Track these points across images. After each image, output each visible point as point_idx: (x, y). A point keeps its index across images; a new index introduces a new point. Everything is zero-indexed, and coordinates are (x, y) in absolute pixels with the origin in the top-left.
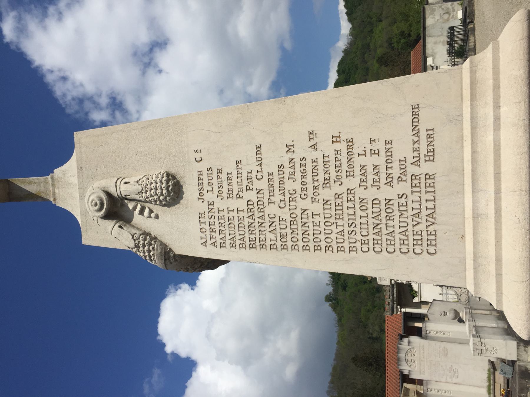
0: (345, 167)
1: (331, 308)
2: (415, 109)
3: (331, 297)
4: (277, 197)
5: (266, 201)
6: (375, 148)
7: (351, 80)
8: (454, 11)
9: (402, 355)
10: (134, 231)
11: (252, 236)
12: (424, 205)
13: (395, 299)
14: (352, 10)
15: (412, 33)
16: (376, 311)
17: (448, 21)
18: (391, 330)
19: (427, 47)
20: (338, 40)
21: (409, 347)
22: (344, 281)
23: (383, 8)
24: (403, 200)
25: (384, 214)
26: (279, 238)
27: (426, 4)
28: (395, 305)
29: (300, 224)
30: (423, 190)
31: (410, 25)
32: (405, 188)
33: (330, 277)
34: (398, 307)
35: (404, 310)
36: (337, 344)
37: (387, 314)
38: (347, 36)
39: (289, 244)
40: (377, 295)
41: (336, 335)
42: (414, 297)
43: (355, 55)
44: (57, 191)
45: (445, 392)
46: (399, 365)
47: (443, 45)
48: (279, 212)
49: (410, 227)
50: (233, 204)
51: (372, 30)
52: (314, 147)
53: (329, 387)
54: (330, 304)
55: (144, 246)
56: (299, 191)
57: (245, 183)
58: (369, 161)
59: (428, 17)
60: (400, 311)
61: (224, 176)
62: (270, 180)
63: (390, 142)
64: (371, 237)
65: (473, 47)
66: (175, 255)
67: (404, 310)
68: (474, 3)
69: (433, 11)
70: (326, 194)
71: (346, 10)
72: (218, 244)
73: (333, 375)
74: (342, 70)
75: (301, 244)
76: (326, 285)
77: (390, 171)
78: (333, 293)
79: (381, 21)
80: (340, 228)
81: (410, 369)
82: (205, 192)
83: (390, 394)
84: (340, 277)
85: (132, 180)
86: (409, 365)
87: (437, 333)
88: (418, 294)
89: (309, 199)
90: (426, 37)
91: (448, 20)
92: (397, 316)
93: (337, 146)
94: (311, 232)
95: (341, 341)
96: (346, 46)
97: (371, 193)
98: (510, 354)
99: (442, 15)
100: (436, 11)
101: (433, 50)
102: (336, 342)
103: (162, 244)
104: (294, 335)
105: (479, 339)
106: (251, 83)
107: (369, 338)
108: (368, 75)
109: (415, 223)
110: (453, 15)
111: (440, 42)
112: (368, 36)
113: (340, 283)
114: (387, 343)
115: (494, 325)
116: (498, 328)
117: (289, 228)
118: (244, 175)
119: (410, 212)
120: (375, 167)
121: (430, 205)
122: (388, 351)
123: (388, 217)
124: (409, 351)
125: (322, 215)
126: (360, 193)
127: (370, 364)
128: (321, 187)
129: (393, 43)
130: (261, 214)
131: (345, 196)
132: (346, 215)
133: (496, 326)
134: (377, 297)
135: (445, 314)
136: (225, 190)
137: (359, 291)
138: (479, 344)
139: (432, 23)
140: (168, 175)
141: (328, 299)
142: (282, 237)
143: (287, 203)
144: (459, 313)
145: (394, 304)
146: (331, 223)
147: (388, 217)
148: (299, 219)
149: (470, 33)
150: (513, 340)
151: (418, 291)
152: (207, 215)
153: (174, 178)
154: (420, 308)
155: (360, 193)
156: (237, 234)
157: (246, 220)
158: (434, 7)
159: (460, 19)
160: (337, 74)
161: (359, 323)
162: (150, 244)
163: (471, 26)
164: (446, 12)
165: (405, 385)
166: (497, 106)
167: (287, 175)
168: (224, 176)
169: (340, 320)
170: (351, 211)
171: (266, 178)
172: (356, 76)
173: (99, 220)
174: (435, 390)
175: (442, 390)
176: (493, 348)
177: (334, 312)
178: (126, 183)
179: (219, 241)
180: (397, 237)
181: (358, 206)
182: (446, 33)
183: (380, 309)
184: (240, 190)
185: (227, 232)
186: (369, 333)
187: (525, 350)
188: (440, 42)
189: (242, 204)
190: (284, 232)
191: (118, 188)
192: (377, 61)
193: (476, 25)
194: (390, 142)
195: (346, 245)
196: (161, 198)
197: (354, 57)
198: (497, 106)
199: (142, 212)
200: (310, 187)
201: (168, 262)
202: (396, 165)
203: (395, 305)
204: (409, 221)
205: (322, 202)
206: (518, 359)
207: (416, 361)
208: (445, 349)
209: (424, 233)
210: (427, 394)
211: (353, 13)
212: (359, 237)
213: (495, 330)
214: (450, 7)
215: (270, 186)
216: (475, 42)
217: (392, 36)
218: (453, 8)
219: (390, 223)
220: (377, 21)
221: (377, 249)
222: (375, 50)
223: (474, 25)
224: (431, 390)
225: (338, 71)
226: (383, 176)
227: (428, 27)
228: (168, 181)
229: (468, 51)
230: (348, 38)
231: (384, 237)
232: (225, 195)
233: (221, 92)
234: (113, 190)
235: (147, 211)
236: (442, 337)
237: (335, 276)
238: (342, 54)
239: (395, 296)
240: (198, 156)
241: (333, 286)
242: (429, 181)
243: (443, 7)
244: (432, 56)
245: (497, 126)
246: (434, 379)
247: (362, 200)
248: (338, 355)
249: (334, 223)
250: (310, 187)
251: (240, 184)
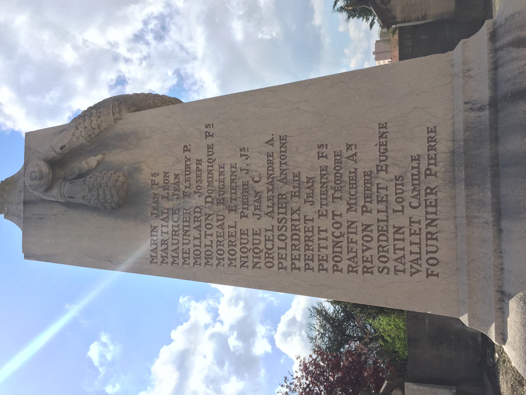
109: (414, 270)
146: (259, 249)
249: (250, 249)
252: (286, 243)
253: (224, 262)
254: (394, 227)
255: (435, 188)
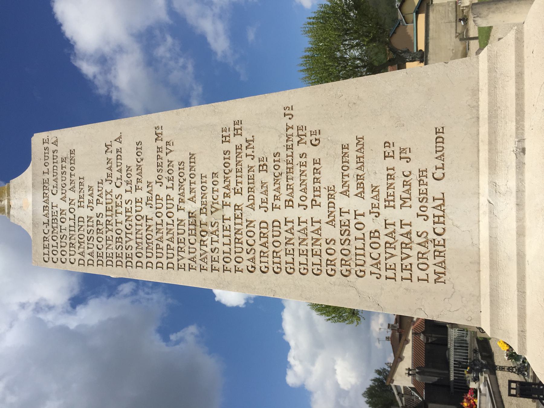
252: (75, 215)
253: (152, 246)
254: (247, 221)
255: (241, 205)
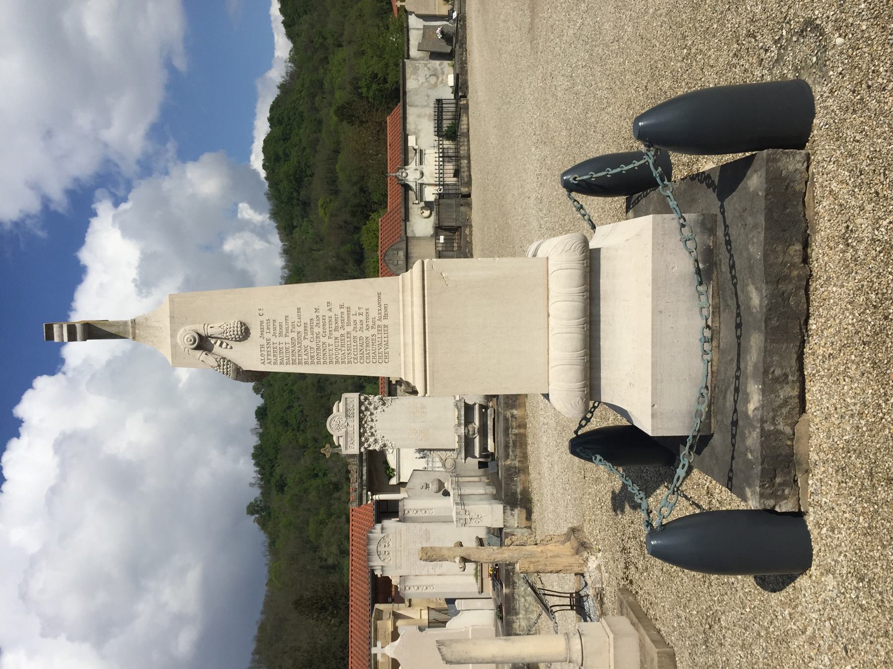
0: (346, 321)
1: (257, 525)
2: (379, 295)
3: (258, 506)
4: (309, 336)
5: (302, 338)
6: (361, 312)
7: (292, 137)
8: (443, 73)
9: (373, 547)
10: (216, 357)
11: (294, 358)
12: (383, 339)
13: (364, 482)
14: (294, 18)
15: (389, 80)
16: (333, 522)
17: (435, 86)
18: (357, 534)
19: (408, 121)
20: (269, 67)
21: (383, 535)
22: (281, 476)
23: (344, 25)
24: (374, 337)
25: (365, 344)
26: (310, 358)
27: (406, 58)
28: (364, 492)
29: (322, 350)
30: (383, 332)
31: (387, 66)
32: (375, 331)
33: (256, 472)
34: (369, 493)
35: (377, 497)
36: (267, 584)
37: (353, 506)
38: (286, 62)
39: (316, 361)
40: (336, 495)
41: (265, 570)
42: (391, 477)
43: (299, 95)
44: (137, 331)
45: (427, 588)
46: (369, 560)
47: (430, 121)
48: (310, 344)
49: (377, 350)
50: (283, 340)
51: (326, 58)
52: (330, 310)
53: (253, 661)
54: (256, 517)
55: (224, 365)
56: (322, 333)
57: (290, 328)
58: (358, 318)
59: (410, 78)
60: (372, 499)
61: (277, 324)
62: (305, 327)
63: (368, 309)
64: (358, 356)
65: (466, 131)
66: (243, 370)
67: (377, 497)
68: (467, 71)
69: (416, 69)
70: (336, 334)
71: (283, 18)
72: (272, 363)
73: (259, 640)
74: (278, 118)
75: (322, 361)
76: (248, 486)
77: (368, 323)
78: (261, 498)
79: (340, 46)
80: (343, 352)
81: (383, 564)
82: (265, 333)
83: (355, 631)
84: (274, 470)
85: (216, 325)
86: (382, 559)
87: (417, 512)
88: (395, 473)
89: (327, 337)
90: (407, 106)
91: (435, 85)
92: (367, 507)
93: (342, 310)
94: (328, 354)
95: (274, 579)
96: (283, 79)
97: (359, 334)
98: (496, 521)
99: (427, 76)
100: (420, 70)
101: (416, 125)
102: (266, 581)
103: (235, 364)
104: (193, 577)
105: (463, 506)
106: (108, 125)
107: (321, 567)
108: (320, 131)
110: (442, 80)
111: (425, 115)
112: (321, 67)
113: (273, 480)
114: (352, 555)
115: (482, 491)
116: (486, 494)
117: (315, 352)
118: (290, 324)
119: (377, 343)
120: (361, 321)
121: (386, 339)
122: (353, 568)
123: (367, 346)
124: (382, 540)
125: (334, 345)
126: (353, 334)
127: (323, 608)
128: (333, 331)
129: (360, 88)
130: (299, 345)
131: (346, 335)
132: (346, 345)
133: (484, 493)
134: (335, 499)
135: (427, 486)
136: (278, 331)
137: (306, 491)
138: (463, 512)
139: (414, 87)
140: (241, 323)
141: (252, 509)
142: (312, 357)
143: (315, 339)
144: (444, 483)
145: (362, 489)
147: (367, 346)
148: (321, 347)
149: (462, 110)
150: (499, 504)
151: (395, 468)
152: (265, 346)
153: (245, 325)
154: (398, 492)
155: (353, 334)
156: (285, 357)
157: (291, 348)
158: (416, 63)
159: (451, 87)
160: (269, 124)
161: (305, 545)
162: (228, 364)
163: (463, 102)
164: (433, 73)
165: (377, 606)
166: (412, 297)
167: (315, 324)
168: (277, 324)
169: (272, 544)
170: (349, 343)
171: (303, 325)
172: (301, 131)
173: (190, 350)
174: (414, 588)
175: (423, 586)
176: (478, 516)
177: (262, 532)
178: (211, 327)
179: (273, 361)
180: (371, 355)
181: (352, 340)
182: (432, 104)
183: (340, 517)
184: (287, 332)
185: (278, 356)
186: (321, 558)
187: (512, 515)
188: (425, 115)
189: (288, 340)
190: (312, 354)
191: (206, 330)
192: (336, 112)
193: (469, 102)
194: (368, 309)
195: (346, 360)
196: (237, 336)
197: (297, 99)
198: (412, 297)
199: (221, 345)
200: (328, 330)
201: (238, 375)
202: (371, 320)
203: (364, 492)
204: (377, 347)
205: (334, 338)
206: (504, 525)
207: (390, 553)
208: (427, 532)
209: (383, 353)
210: (404, 594)
211: (295, 24)
212: (353, 356)
213: (482, 496)
214: (439, 68)
215: (305, 330)
216: (468, 125)
217: (358, 75)
218: (442, 69)
219: (368, 348)
220: (334, 44)
221: (362, 361)
222: (332, 92)
223: (467, 101)
224: (410, 588)
225: (270, 120)
226: (365, 325)
227: (410, 91)
228: (242, 326)
229: (460, 135)
230: (287, 66)
231: (365, 356)
232: (277, 335)
233: (48, 134)
234: (202, 332)
235: (224, 345)
236: (422, 517)
237: (265, 469)
238: (276, 92)
239: (364, 477)
240: (261, 312)
241: (261, 487)
242: (386, 328)
243: (429, 65)
244: (415, 133)
245: (412, 305)
246: (413, 573)
247: (354, 337)
248: (270, 604)
250: (328, 330)
251: (287, 329)
